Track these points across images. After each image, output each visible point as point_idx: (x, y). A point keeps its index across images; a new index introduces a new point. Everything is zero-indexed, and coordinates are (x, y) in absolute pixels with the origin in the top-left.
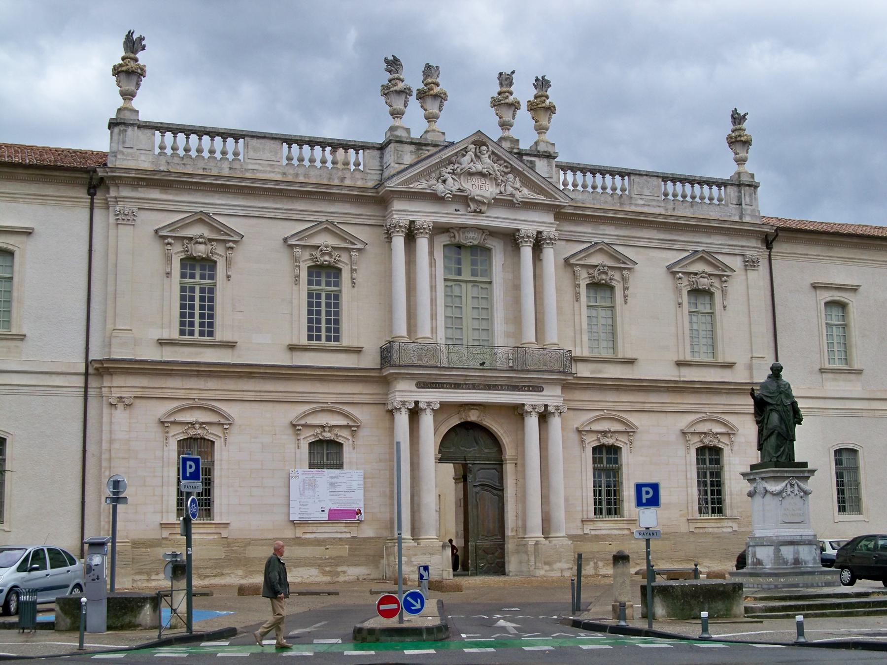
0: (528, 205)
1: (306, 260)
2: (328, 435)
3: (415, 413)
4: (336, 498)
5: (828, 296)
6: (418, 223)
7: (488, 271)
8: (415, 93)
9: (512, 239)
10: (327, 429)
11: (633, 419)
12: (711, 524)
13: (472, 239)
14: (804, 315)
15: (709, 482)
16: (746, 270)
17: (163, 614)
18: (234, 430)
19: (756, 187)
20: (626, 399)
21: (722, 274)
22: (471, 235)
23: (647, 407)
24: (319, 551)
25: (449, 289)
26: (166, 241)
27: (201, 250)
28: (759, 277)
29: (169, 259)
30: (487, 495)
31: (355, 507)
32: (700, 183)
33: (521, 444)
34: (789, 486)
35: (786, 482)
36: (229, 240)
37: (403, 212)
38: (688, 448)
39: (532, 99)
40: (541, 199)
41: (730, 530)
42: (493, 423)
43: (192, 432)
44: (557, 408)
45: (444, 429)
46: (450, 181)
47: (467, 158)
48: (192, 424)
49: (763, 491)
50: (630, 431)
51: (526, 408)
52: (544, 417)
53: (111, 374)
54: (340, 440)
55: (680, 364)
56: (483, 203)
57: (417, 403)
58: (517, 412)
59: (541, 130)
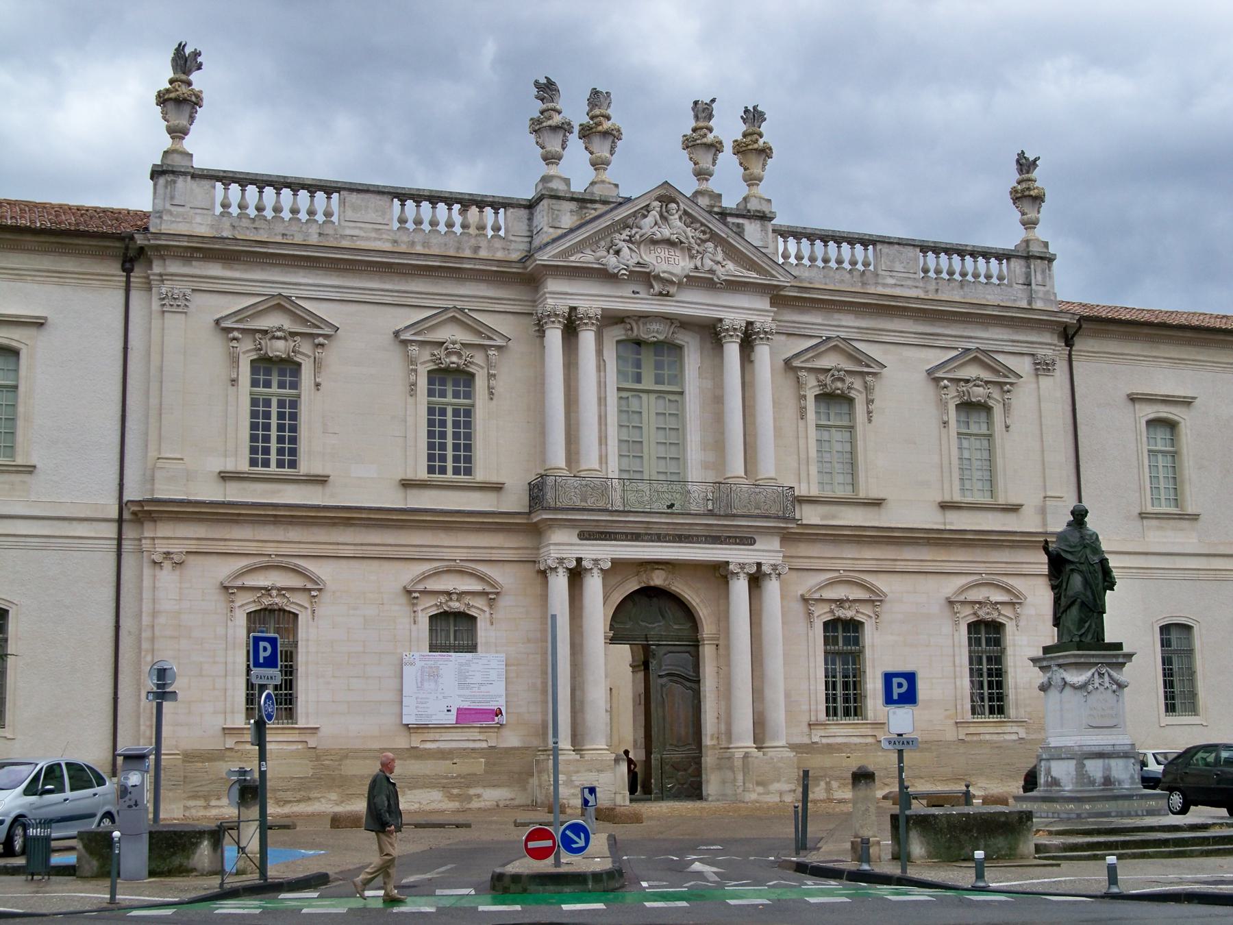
0: (734, 286)
2: (456, 605)
3: (576, 575)
4: (467, 692)
5: (1151, 411)
6: (581, 310)
7: (678, 377)
8: (576, 129)
9: (712, 332)
10: (454, 597)
11: (880, 583)
12: (988, 729)
13: (656, 332)
14: (1118, 438)
15: (985, 670)
16: (1037, 375)
17: (226, 854)
18: (326, 598)
19: (1051, 260)
20: (870, 555)
21: (1004, 381)
22: (655, 327)
23: (900, 566)
24: (443, 767)
25: (623, 402)
27: (279, 348)
28: (1054, 385)
29: (234, 360)
30: (677, 688)
31: (493, 706)
32: (974, 254)
33: (724, 617)
34: (1096, 676)
35: (1093, 670)
36: (319, 334)
37: (560, 295)
38: (957, 623)
39: (739, 137)
40: (752, 277)
41: (1014, 737)
42: (685, 589)
43: (266, 601)
44: (775, 567)
45: (618, 597)
46: (625, 251)
47: (649, 220)
48: (267, 590)
49: (1061, 683)
50: (876, 600)
51: (731, 567)
52: (756, 580)
53: (154, 521)
54: (473, 612)
55: (945, 506)
56: (672, 282)
57: (579, 560)
58: (719, 573)
59: (752, 180)
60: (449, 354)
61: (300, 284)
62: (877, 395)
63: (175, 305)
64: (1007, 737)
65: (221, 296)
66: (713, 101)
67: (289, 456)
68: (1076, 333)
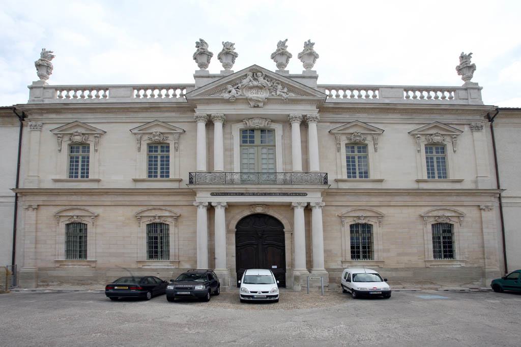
1: (344, 140)
3: (211, 209)
6: (213, 115)
9: (287, 122)
11: (383, 211)
12: (444, 263)
15: (442, 241)
16: (472, 132)
20: (375, 201)
22: (257, 121)
23: (392, 204)
26: (417, 136)
27: (78, 139)
29: (60, 144)
36: (376, 134)
41: (459, 266)
42: (275, 213)
43: (72, 220)
44: (318, 204)
47: (247, 80)
48: (72, 217)
53: (25, 195)
54: (167, 223)
56: (259, 101)
60: (154, 136)
61: (89, 118)
62: (380, 145)
63: (40, 128)
65: (53, 123)
66: (287, 40)
67: (85, 174)
68: (494, 116)
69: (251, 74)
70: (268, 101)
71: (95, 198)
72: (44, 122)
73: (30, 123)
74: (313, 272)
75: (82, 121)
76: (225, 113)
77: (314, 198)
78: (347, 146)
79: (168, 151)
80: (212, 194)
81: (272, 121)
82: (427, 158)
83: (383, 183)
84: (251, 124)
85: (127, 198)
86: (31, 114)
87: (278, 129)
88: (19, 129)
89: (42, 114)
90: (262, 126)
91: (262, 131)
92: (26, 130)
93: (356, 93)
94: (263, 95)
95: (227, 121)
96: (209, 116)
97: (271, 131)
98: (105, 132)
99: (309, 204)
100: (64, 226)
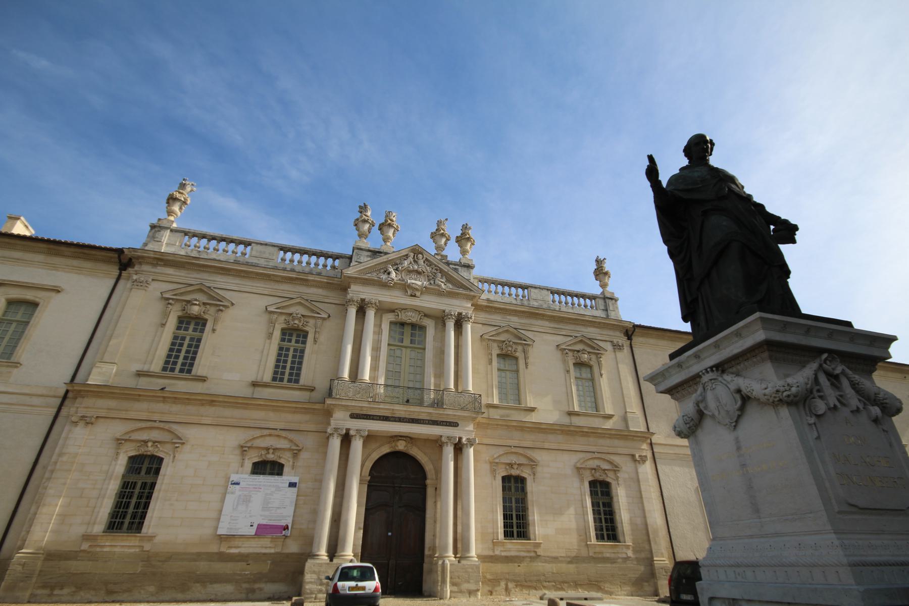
2: (271, 457)
3: (346, 440)
4: (267, 513)
7: (423, 342)
9: (441, 319)
10: (271, 451)
12: (515, 547)
13: (413, 318)
18: (187, 448)
19: (616, 300)
21: (597, 352)
22: (410, 314)
23: (547, 445)
24: (238, 567)
25: (392, 352)
27: (195, 310)
29: (166, 315)
31: (283, 523)
33: (438, 471)
34: (823, 379)
35: (814, 366)
36: (220, 305)
37: (358, 292)
38: (582, 480)
43: (142, 451)
45: (376, 456)
46: (393, 275)
49: (731, 404)
50: (533, 464)
51: (443, 439)
52: (459, 448)
56: (417, 289)
57: (348, 430)
58: (437, 444)
59: (464, 252)
60: (294, 319)
61: (219, 281)
64: (117, 550)
67: (188, 367)
69: (412, 255)
70: (426, 291)
71: (192, 409)
72: (155, 278)
73: (135, 277)
74: (335, 561)
75: (208, 285)
76: (380, 299)
77: (466, 431)
78: (284, 332)
79: (304, 343)
80: (354, 416)
81: (426, 315)
82: (281, 349)
83: (206, 385)
84: (404, 317)
85: (238, 413)
86: (140, 264)
87: (430, 325)
88: (113, 282)
89: (155, 266)
90: (414, 320)
91: (413, 326)
92: (122, 283)
93: (314, 259)
94: (419, 282)
95: (382, 310)
96: (363, 300)
97: (423, 328)
98: (233, 304)
99: (348, 430)
100: (126, 458)
